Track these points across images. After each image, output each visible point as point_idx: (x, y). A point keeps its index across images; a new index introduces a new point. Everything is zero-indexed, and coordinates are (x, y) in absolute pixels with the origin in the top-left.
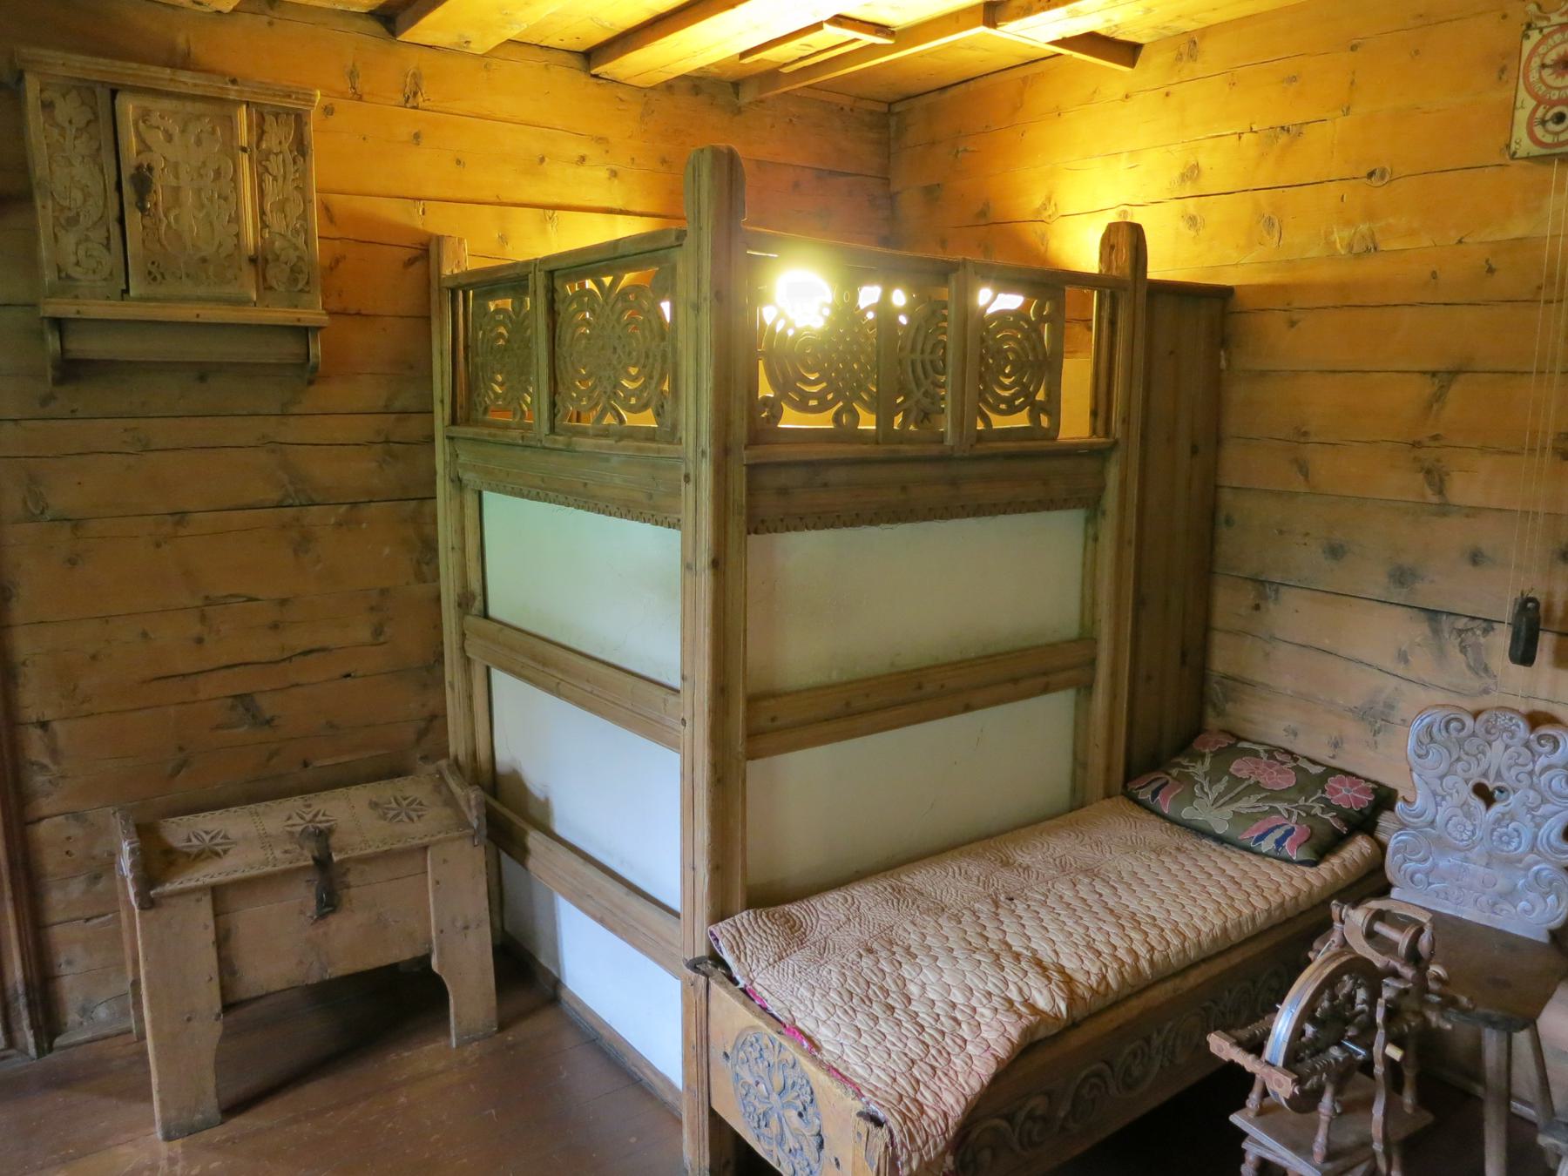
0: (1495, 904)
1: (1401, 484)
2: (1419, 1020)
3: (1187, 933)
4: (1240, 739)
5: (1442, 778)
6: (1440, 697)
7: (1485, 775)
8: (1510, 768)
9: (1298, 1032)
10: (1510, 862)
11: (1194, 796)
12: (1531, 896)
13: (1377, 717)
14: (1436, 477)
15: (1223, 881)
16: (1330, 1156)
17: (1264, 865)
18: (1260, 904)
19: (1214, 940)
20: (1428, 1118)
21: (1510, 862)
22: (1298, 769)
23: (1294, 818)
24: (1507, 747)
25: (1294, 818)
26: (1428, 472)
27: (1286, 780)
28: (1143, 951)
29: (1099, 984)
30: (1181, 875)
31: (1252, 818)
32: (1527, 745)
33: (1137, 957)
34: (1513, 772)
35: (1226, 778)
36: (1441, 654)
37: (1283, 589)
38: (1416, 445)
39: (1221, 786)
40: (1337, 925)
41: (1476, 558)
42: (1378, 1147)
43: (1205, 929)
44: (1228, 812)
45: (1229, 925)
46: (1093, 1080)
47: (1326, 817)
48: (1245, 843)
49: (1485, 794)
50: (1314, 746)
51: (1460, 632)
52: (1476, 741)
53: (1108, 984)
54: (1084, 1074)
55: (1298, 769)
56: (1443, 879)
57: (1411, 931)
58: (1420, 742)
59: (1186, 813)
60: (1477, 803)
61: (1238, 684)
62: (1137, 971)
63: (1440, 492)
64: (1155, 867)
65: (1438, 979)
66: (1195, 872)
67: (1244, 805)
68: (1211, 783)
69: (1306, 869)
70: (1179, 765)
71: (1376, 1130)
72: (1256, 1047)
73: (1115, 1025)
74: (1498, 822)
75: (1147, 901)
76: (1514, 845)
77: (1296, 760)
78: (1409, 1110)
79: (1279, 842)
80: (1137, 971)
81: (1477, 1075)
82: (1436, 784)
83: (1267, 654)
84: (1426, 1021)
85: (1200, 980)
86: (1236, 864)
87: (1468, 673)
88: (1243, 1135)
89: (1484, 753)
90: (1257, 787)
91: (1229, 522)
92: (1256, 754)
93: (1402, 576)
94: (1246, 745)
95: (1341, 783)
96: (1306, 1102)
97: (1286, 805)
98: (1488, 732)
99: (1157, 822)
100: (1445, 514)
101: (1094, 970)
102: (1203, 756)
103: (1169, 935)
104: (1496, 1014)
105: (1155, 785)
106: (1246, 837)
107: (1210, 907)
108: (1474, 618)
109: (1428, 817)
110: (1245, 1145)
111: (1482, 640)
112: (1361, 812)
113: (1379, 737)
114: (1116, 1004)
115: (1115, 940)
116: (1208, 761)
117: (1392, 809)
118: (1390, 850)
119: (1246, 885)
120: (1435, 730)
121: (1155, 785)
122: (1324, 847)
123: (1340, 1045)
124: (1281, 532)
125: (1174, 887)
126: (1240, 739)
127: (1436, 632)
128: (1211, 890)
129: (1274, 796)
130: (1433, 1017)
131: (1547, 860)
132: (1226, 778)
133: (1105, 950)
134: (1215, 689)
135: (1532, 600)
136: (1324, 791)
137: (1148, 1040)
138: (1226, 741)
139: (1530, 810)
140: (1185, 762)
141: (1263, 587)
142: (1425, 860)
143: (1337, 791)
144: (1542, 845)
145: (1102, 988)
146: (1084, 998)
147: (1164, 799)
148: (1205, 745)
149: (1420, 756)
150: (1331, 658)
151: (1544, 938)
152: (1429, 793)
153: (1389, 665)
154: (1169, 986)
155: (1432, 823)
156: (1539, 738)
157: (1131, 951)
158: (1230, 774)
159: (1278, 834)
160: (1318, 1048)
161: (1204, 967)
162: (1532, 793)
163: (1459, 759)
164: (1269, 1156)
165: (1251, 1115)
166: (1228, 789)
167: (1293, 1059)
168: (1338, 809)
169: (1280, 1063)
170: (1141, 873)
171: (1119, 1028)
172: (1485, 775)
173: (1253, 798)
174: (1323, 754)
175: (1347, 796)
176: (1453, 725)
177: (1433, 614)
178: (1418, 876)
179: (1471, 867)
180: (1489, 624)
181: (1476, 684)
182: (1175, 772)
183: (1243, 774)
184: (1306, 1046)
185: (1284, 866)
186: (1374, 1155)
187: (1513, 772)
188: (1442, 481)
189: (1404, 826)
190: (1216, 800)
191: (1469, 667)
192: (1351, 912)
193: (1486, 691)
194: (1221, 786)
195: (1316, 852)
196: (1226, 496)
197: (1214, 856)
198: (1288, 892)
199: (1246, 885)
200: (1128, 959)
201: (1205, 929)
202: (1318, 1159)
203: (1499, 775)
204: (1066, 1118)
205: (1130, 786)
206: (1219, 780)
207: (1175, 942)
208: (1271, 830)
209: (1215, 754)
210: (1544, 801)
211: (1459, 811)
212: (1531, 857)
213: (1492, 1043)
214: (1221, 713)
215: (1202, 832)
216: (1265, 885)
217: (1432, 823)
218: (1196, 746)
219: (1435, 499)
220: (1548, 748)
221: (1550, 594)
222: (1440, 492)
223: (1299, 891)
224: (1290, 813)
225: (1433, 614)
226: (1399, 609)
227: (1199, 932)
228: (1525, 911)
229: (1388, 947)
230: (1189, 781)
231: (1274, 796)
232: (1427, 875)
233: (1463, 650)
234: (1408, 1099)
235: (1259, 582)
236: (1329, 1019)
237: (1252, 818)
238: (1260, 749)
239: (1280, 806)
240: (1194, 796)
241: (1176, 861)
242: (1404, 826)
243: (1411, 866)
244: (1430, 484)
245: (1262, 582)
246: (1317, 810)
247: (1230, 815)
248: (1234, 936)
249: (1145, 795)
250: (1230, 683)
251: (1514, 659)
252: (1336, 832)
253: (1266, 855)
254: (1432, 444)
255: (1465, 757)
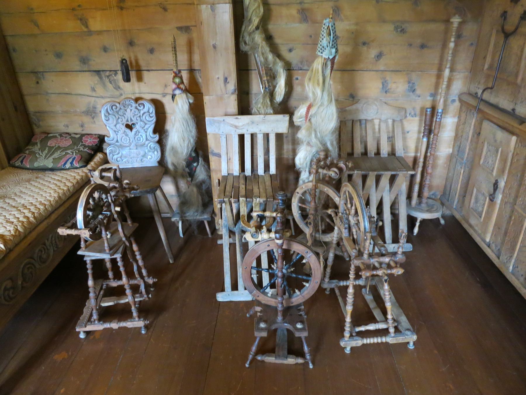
0: (142, 160)
1: (72, 25)
2: (124, 197)
3: (46, 203)
4: (48, 134)
5: (115, 126)
6: (109, 100)
7: (127, 121)
8: (134, 117)
9: (85, 216)
10: (143, 145)
11: (37, 158)
12: (150, 153)
13: (92, 113)
14: (85, 22)
15: (55, 182)
16: (110, 249)
17: (68, 172)
18: (69, 184)
19: (57, 202)
20: (136, 225)
21: (143, 145)
22: (72, 138)
23: (74, 154)
24: (131, 110)
25: (74, 154)
26: (81, 20)
27: (69, 142)
28: (30, 215)
29: (15, 233)
30: (39, 186)
31: (60, 158)
32: (136, 108)
33: (28, 218)
34: (135, 118)
35: (47, 148)
36: (104, 85)
37: (45, 74)
38: (73, 9)
39: (46, 151)
40: (91, 179)
41: (105, 49)
42: (124, 239)
43: (52, 199)
44: (51, 159)
45: (60, 195)
46: (29, 266)
47: (85, 150)
48: (60, 168)
49: (129, 127)
50: (75, 129)
51: (108, 77)
52: (122, 111)
53: (19, 231)
54: (22, 266)
55: (72, 138)
56: (126, 157)
57: (113, 171)
58: (105, 116)
59: (36, 165)
60: (128, 131)
61: (41, 114)
62: (29, 222)
63: (87, 27)
64: (28, 186)
65: (127, 184)
66: (44, 183)
67: (56, 155)
68: (42, 152)
69: (83, 169)
70: (28, 149)
71: (122, 235)
72: (74, 226)
73: (27, 244)
74: (135, 134)
75: (27, 198)
76: (142, 140)
77: (70, 135)
78: (131, 225)
79: (71, 163)
80: (29, 222)
81: (151, 211)
82: (114, 128)
83: (48, 100)
84: (126, 197)
85: (56, 217)
86: (59, 175)
87: (115, 90)
88: (83, 256)
89: (125, 114)
90: (59, 148)
91: (14, 50)
92: (56, 137)
93: (84, 61)
94: (51, 135)
95: (87, 138)
96: (96, 236)
97: (71, 150)
98: (124, 107)
99: (27, 171)
100: (91, 35)
101: (12, 229)
102: (37, 143)
103: (39, 206)
104: (148, 189)
105: (21, 159)
106: (59, 165)
107: (52, 192)
108: (111, 71)
109: (115, 140)
110: (85, 259)
111: (115, 78)
112: (96, 145)
113: (95, 119)
114: (25, 237)
115: (17, 216)
116: (39, 144)
117: (105, 142)
118: (108, 154)
119: (64, 180)
120: (109, 111)
121: (21, 159)
122: (87, 160)
123: (101, 214)
124: (36, 51)
125: (37, 190)
126: (48, 134)
127: (101, 78)
128: (51, 186)
129: (66, 149)
130: (128, 195)
131: (151, 142)
132: (47, 148)
133: (15, 221)
134: (33, 118)
135: (125, 59)
136: (82, 142)
137: (45, 244)
138: (44, 136)
139: (143, 128)
140: (30, 147)
141: (37, 75)
142: (119, 153)
143: (87, 141)
144: (149, 138)
145: (17, 233)
146: (10, 240)
147: (26, 162)
148: (36, 139)
149: (107, 120)
150: (69, 96)
151: (157, 165)
152: (111, 129)
153: (89, 93)
154: (45, 223)
155: (117, 141)
156: (139, 105)
157: (25, 217)
158: (48, 147)
159: (70, 160)
160: (95, 217)
161: (56, 212)
162: (142, 123)
163: (119, 118)
164: (93, 258)
165: (84, 249)
166: (49, 152)
167: (87, 224)
168: (88, 146)
169: (83, 227)
170: (24, 190)
171: (30, 244)
172: (127, 121)
173: (59, 152)
174: (79, 130)
175: (90, 142)
176: (114, 107)
177: (98, 72)
178: (118, 159)
179: (132, 151)
180: (116, 72)
181: (117, 93)
182: (27, 152)
183: (53, 145)
184: (91, 219)
185: (76, 170)
186: (124, 243)
187: (135, 118)
188: (86, 22)
189: (109, 145)
190: (45, 157)
191: (114, 88)
192: (94, 173)
193: (121, 95)
194: (46, 151)
195: (85, 162)
196: (9, 40)
197: (50, 176)
198: (78, 178)
199: (64, 180)
200: (25, 220)
201: (52, 199)
202: (107, 251)
203: (131, 120)
204: (22, 283)
205: (11, 162)
206: (45, 149)
207: (42, 207)
208: (68, 160)
209: (41, 141)
210: (146, 124)
211: (124, 135)
212: (147, 142)
213: (150, 198)
214: (39, 127)
215: (44, 170)
216: (68, 179)
217: (117, 141)
218: (33, 140)
219: (86, 30)
220: (142, 107)
221: (130, 58)
222: (87, 27)
223: (82, 176)
224: (73, 153)
225: (98, 72)
226: (87, 73)
227: (50, 201)
228: (150, 159)
229: (108, 180)
230: (34, 153)
231: (66, 149)
232: (121, 158)
233: (111, 83)
234: (129, 222)
235: (35, 73)
236: (96, 208)
237: (60, 158)
238: (57, 135)
239: (69, 151)
240: (37, 158)
241: (36, 182)
242: (109, 145)
243: (115, 157)
244: (83, 24)
245: (36, 73)
246: (82, 149)
247: (52, 160)
248: (64, 198)
249: (18, 164)
250: (38, 114)
251: (124, 81)
252: (89, 154)
253: (69, 169)
254: (78, 8)
255: (120, 117)
